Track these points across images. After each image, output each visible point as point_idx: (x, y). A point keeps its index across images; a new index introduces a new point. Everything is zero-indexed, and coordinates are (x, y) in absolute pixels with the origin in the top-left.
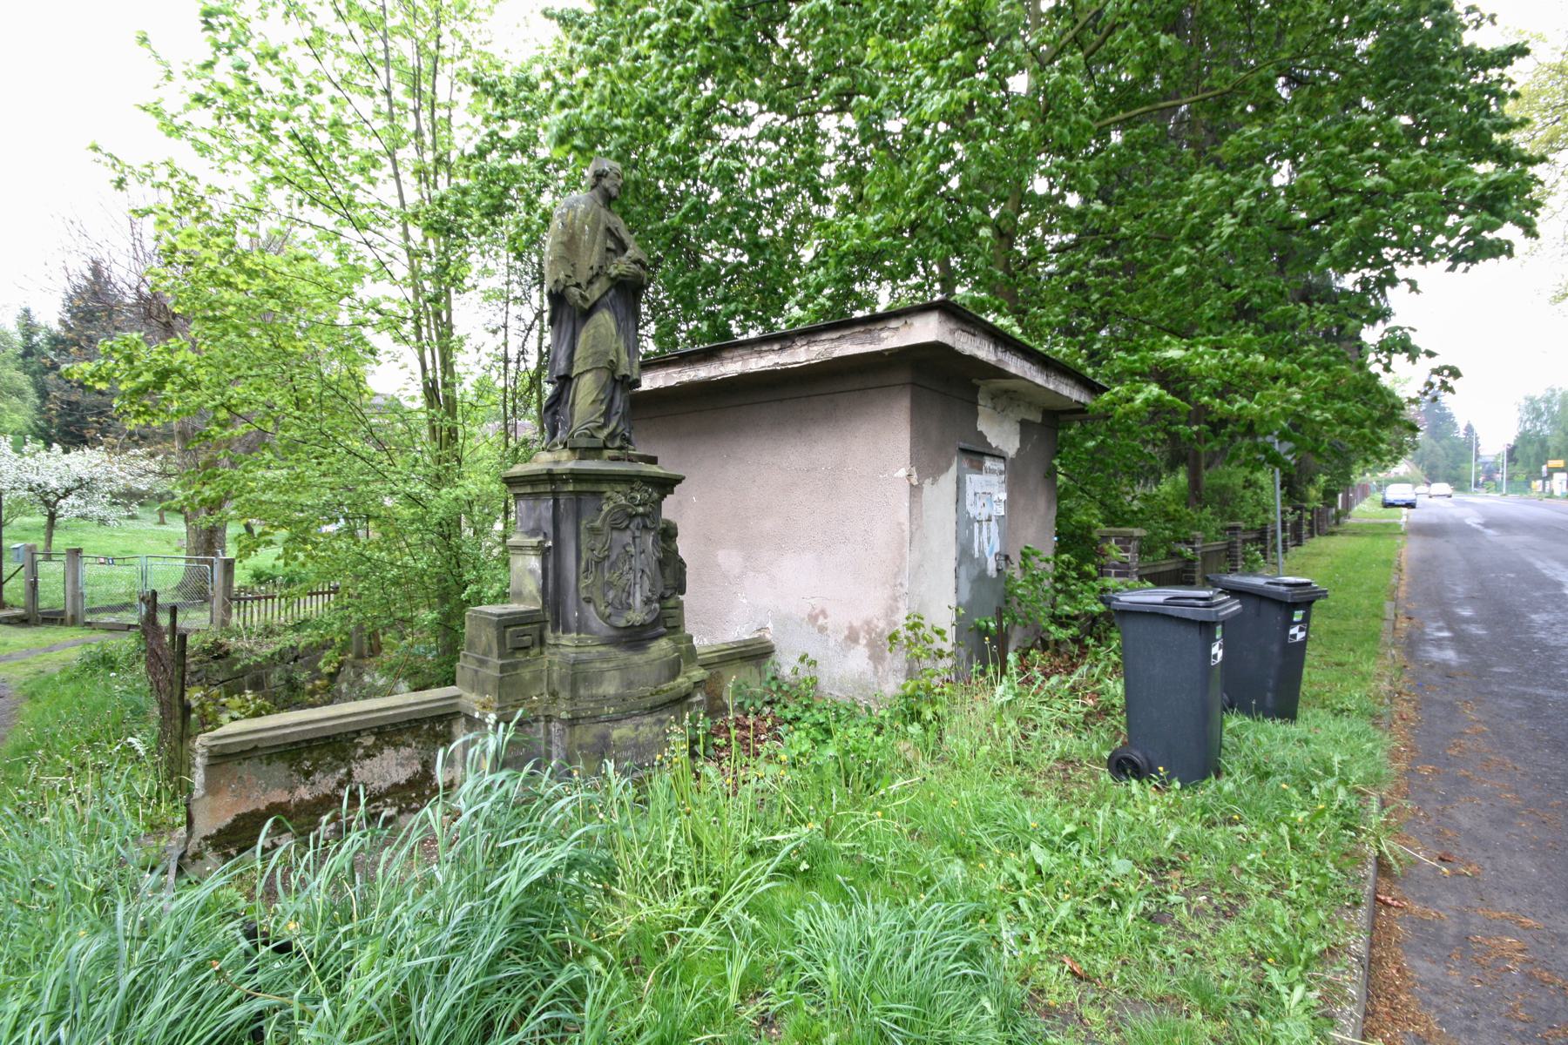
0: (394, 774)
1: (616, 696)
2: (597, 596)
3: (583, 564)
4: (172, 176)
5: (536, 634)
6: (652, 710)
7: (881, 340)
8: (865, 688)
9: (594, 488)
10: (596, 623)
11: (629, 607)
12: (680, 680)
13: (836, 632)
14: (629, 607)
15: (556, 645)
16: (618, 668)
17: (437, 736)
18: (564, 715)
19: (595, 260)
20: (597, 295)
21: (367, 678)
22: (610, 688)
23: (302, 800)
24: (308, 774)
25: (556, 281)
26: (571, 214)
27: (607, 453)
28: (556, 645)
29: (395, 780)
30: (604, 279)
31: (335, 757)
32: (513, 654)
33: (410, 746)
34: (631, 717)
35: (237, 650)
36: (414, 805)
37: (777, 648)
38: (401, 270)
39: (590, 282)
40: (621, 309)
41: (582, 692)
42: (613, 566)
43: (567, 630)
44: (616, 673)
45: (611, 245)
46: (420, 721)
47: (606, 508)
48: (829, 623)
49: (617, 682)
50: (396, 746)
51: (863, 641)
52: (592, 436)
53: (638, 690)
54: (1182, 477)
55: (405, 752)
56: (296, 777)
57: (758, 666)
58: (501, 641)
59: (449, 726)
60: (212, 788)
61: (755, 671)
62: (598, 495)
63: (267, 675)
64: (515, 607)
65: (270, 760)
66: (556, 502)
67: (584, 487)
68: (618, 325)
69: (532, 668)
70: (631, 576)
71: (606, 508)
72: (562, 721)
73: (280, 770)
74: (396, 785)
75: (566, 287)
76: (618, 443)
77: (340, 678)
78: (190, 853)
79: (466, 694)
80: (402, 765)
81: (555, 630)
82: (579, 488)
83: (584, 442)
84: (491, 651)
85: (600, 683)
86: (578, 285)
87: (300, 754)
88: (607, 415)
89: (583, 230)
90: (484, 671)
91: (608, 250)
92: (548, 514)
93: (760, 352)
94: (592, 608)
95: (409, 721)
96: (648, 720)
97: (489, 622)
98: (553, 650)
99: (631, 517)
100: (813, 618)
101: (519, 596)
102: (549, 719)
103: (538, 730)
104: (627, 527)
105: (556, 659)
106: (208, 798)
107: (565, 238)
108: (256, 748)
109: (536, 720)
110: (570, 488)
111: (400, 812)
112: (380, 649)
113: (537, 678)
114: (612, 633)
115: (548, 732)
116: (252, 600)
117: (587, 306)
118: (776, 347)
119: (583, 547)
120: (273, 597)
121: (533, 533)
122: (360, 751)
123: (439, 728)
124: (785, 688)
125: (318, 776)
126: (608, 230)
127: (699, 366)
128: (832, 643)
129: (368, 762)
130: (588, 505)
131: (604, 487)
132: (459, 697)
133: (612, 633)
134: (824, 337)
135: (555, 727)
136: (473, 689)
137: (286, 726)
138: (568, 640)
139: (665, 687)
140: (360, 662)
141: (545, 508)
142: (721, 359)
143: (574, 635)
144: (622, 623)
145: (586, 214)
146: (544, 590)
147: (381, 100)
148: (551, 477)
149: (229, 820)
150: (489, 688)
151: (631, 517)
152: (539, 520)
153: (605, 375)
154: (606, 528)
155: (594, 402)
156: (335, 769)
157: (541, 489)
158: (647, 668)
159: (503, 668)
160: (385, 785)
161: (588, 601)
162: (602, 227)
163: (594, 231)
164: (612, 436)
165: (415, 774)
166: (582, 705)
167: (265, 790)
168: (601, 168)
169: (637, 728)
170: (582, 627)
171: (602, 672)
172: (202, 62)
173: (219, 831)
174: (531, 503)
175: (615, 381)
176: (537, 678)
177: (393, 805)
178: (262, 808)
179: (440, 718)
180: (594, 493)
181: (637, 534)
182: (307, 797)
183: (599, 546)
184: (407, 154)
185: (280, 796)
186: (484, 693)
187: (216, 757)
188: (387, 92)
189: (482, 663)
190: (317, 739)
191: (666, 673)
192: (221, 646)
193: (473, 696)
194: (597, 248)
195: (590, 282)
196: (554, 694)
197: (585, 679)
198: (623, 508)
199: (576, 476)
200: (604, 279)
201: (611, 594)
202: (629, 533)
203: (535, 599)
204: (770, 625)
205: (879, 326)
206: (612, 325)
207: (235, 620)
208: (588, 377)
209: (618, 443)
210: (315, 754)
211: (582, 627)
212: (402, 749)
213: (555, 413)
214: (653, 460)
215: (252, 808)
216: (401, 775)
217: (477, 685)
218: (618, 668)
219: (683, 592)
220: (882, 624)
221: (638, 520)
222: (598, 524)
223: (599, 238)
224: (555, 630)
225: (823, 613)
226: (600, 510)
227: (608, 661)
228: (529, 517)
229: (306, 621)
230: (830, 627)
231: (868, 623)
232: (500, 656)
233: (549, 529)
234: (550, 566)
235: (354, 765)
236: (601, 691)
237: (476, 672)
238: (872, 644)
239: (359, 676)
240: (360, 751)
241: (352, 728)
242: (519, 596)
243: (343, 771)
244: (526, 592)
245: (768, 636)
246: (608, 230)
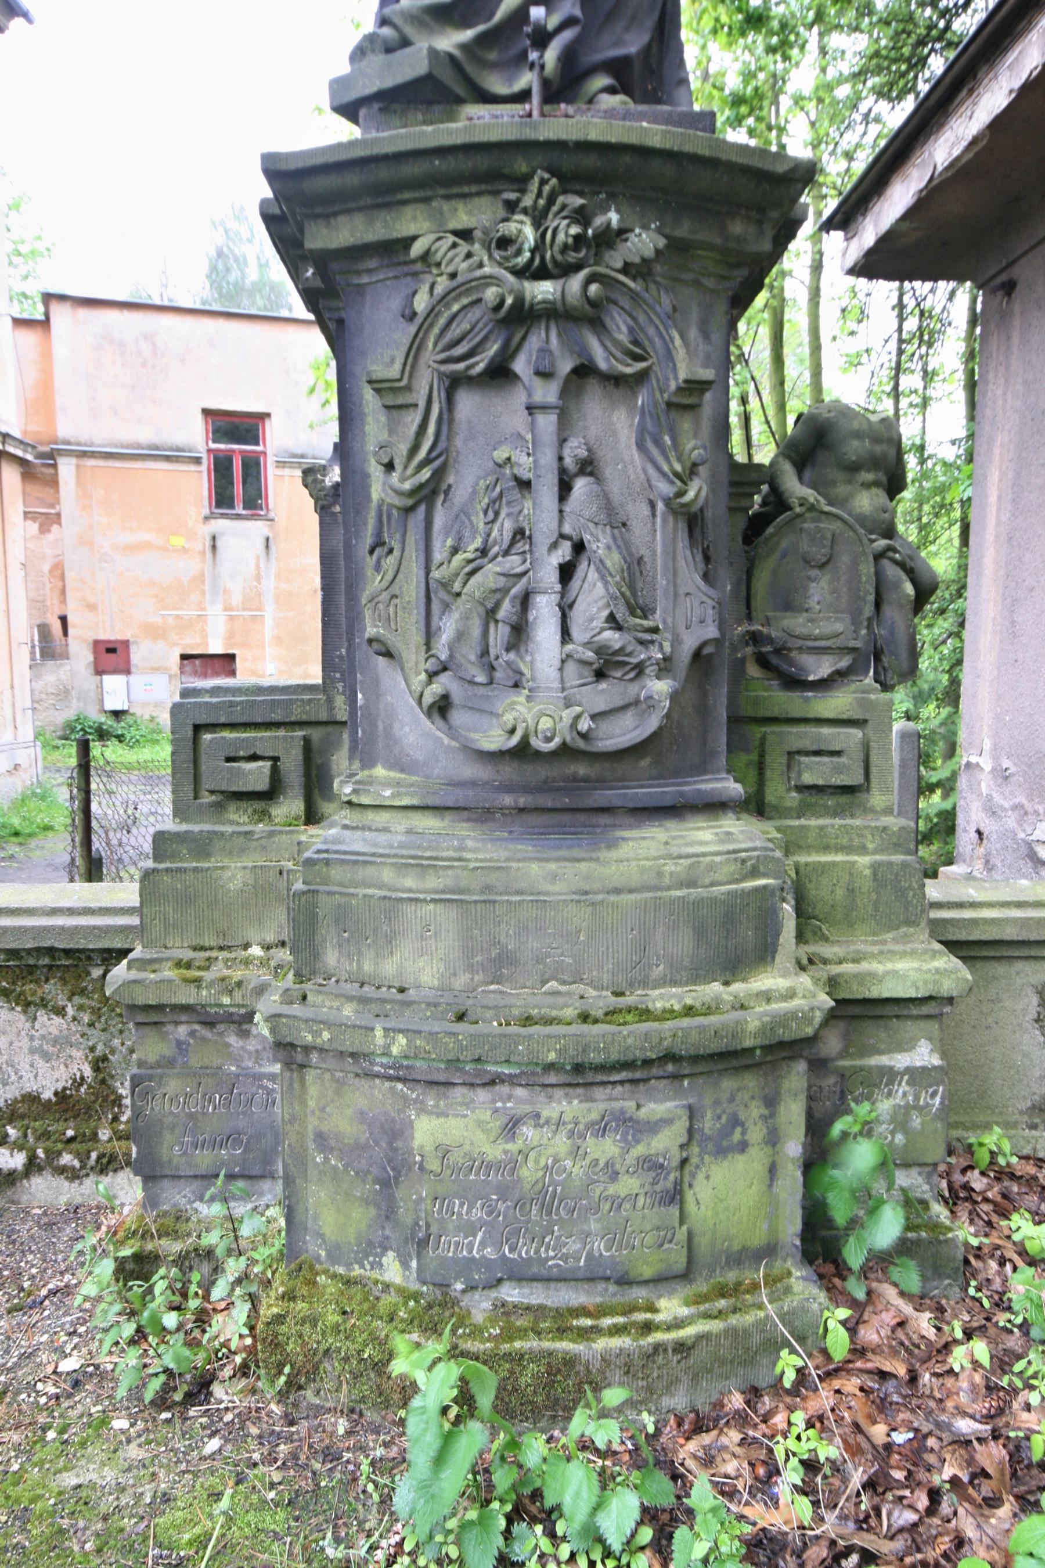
0: (27, 1075)
29: (30, 1086)
32: (219, 807)
33: (60, 1012)
41: (331, 958)
44: (446, 918)
54: (108, 994)
55: (49, 1024)
74: (32, 1098)
80: (47, 1057)
111: (32, 1166)
166: (322, 1004)
169: (511, 1127)
171: (392, 905)
177: (19, 1146)
197: (342, 917)
212: (42, 1016)
236: (389, 968)
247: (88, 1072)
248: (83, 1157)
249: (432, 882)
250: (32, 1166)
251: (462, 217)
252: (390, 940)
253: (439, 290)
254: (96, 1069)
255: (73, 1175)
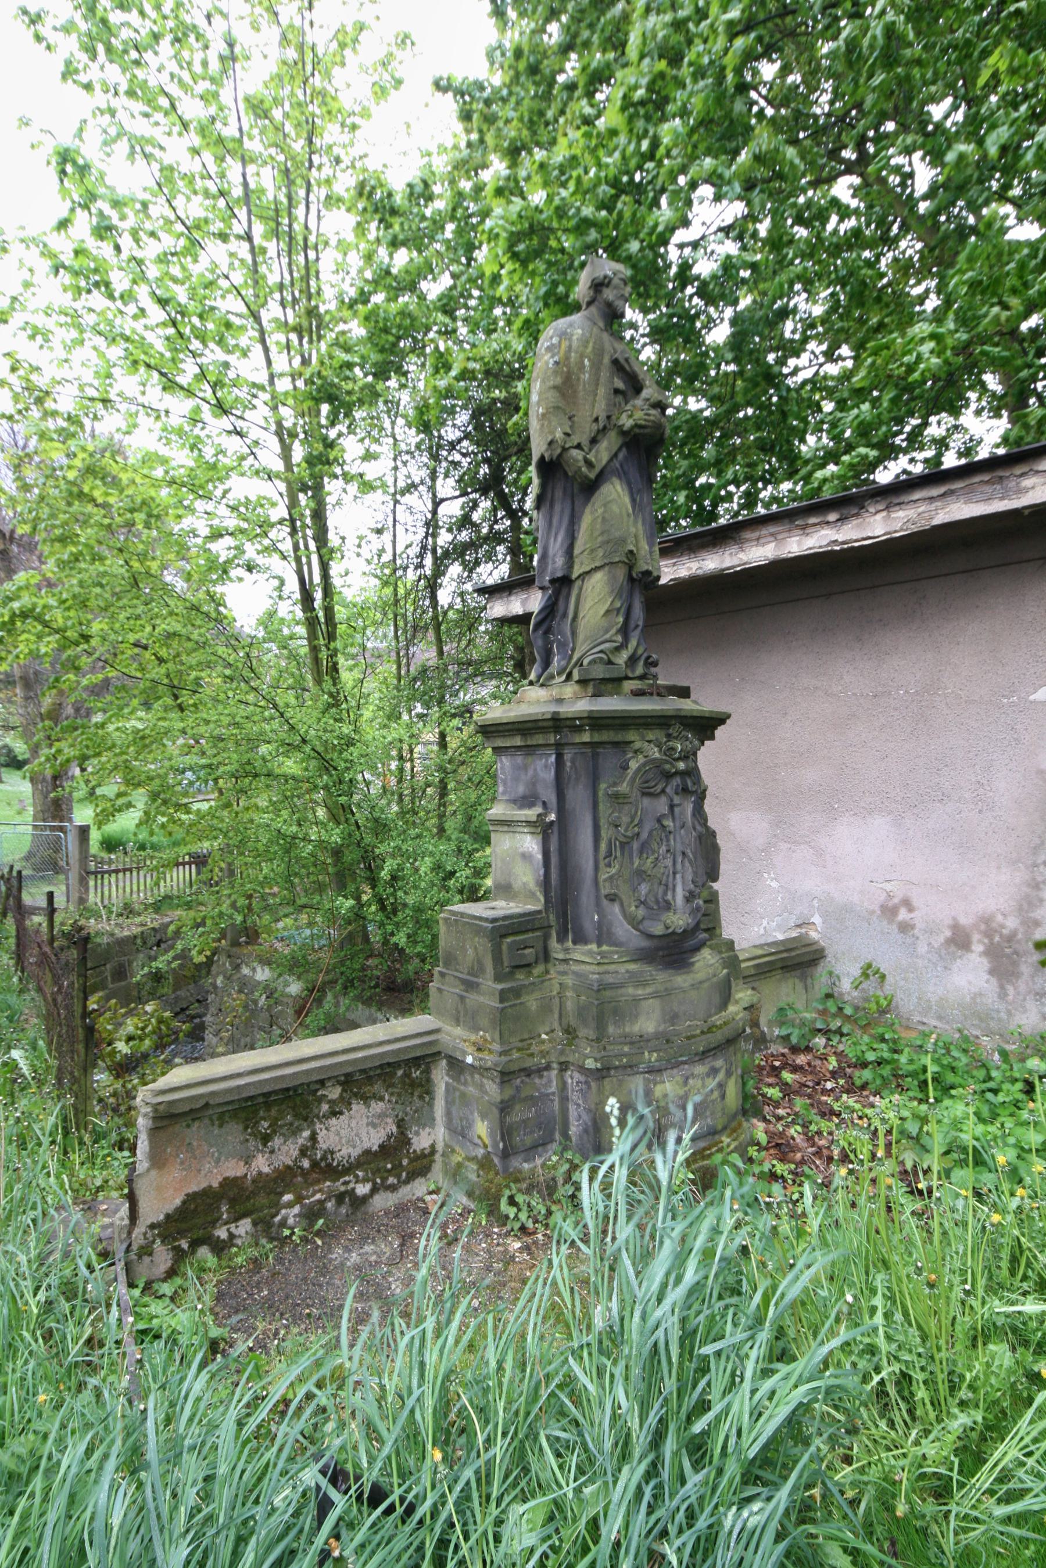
0: (365, 1139)
1: (657, 1036)
2: (624, 891)
3: (603, 846)
4: (13, 369)
5: (540, 945)
6: (704, 1055)
7: (1021, 491)
8: (983, 1017)
9: (619, 737)
10: (623, 930)
11: (668, 906)
12: (732, 1008)
13: (930, 932)
14: (668, 906)
15: (565, 961)
16: (655, 995)
17: (414, 1084)
18: (590, 1064)
19: (600, 408)
20: (605, 457)
21: (245, 971)
22: (648, 1024)
23: (260, 1173)
24: (266, 1139)
25: (551, 443)
26: (564, 345)
27: (629, 686)
28: (565, 961)
29: (366, 1145)
30: (612, 435)
31: (296, 1116)
32: (511, 974)
33: (382, 1099)
34: (677, 1065)
35: (97, 934)
36: (391, 1180)
37: (830, 953)
38: (271, 458)
39: (594, 441)
40: (634, 473)
41: (611, 1029)
42: (643, 848)
43: (580, 939)
45: (620, 384)
46: (395, 1065)
47: (634, 765)
48: (918, 918)
49: (657, 1014)
50: (366, 1099)
51: (978, 948)
52: (610, 662)
53: (684, 1025)
55: (377, 1107)
56: (252, 1143)
57: (803, 978)
58: (497, 958)
59: (427, 1071)
60: (157, 1160)
61: (800, 986)
62: (621, 746)
63: (130, 963)
64: (502, 907)
65: (222, 1120)
66: (559, 757)
67: (605, 736)
68: (633, 500)
69: (537, 995)
70: (669, 862)
71: (634, 765)
72: (582, 1069)
73: (234, 1133)
74: (367, 1152)
75: (564, 449)
76: (640, 670)
77: (214, 969)
78: (135, 1247)
79: (447, 1028)
80: (374, 1126)
81: (561, 939)
82: (597, 738)
83: (599, 672)
84: (482, 969)
85: (635, 1017)
86: (579, 446)
87: (256, 1112)
88: (625, 631)
89: (581, 367)
90: (474, 999)
91: (617, 391)
92: (549, 775)
93: (804, 527)
94: (616, 908)
95: (381, 1066)
96: (700, 1069)
97: (478, 931)
98: (562, 967)
99: (668, 776)
100: (889, 911)
101: (505, 890)
102: (564, 1067)
103: (550, 1081)
104: (663, 791)
105: (569, 981)
106: (154, 1173)
107: (559, 380)
108: (207, 1105)
109: (548, 1067)
110: (586, 737)
111: (374, 1190)
112: (257, 934)
113: (545, 1009)
114: (644, 943)
115: (563, 1086)
116: (110, 872)
117: (592, 475)
118: (832, 517)
119: (603, 822)
120: (130, 870)
121: (526, 801)
122: (325, 1107)
123: (416, 1074)
124: (848, 1011)
125: (277, 1141)
126: (615, 362)
127: (704, 554)
128: (922, 948)
129: (333, 1121)
130: (609, 761)
131: (632, 736)
132: (437, 1031)
133: (644, 943)
134: (917, 495)
135: (573, 1078)
136: (457, 1022)
137: (239, 1075)
138: (579, 953)
139: (717, 1019)
140: (235, 950)
141: (544, 767)
142: (740, 542)
143: (593, 947)
144: (658, 929)
145: (585, 343)
146: (546, 883)
147: (243, 250)
148: (557, 723)
149: (178, 1202)
150: (484, 1022)
151: (668, 776)
152: (533, 783)
153: (621, 573)
154: (636, 793)
155: (608, 612)
156: (296, 1132)
157: (539, 739)
158: (693, 994)
159: (503, 996)
160: (355, 1153)
161: (612, 898)
162: (606, 360)
163: (596, 366)
164: (633, 660)
165: (389, 1137)
167: (218, 1161)
168: (600, 274)
170: (603, 936)
171: (637, 1001)
172: (54, 222)
173: (168, 1216)
174: (519, 760)
175: (631, 579)
176: (545, 1009)
178: (215, 1185)
179: (416, 1061)
180: (616, 744)
181: (677, 800)
182: (266, 1170)
183: (625, 819)
184: (272, 312)
185: (234, 1169)
186: (476, 1029)
187: (162, 1118)
188: (249, 238)
189: (470, 986)
190: (275, 1092)
191: (717, 999)
192: (81, 928)
193: (458, 1031)
194: (601, 391)
195: (594, 441)
196: (570, 1032)
197: (616, 1012)
198: (657, 764)
199: (596, 721)
200: (612, 435)
201: (644, 889)
202: (663, 799)
203: (533, 894)
204: (817, 919)
205: (1018, 471)
206: (627, 500)
207: (92, 898)
208: (599, 576)
209: (640, 670)
210: (274, 1112)
211: (603, 936)
212: (373, 1103)
213: (547, 632)
214: (684, 692)
215: (204, 1185)
216: (374, 1139)
217: (463, 1016)
218: (655, 995)
219: (715, 879)
220: (1012, 923)
221: (677, 781)
222: (624, 788)
223: (605, 374)
224: (561, 939)
225: (907, 903)
226: (625, 768)
227: (644, 984)
228: (516, 779)
229: (167, 897)
230: (920, 925)
231: (987, 920)
232: (498, 978)
233: (551, 798)
234: (553, 847)
235: (318, 1126)
237: (462, 998)
238: (993, 952)
239: (237, 967)
240: (325, 1107)
241: (315, 1077)
242: (505, 890)
243: (306, 1134)
244: (517, 885)
245: (814, 935)
246: (615, 362)
247: (394, 1129)
248: (399, 1176)
249: (649, 990)
250: (374, 1190)
251: (651, 735)
252: (636, 1016)
253: (287, 546)
254: (399, 1127)
255: (393, 1188)
